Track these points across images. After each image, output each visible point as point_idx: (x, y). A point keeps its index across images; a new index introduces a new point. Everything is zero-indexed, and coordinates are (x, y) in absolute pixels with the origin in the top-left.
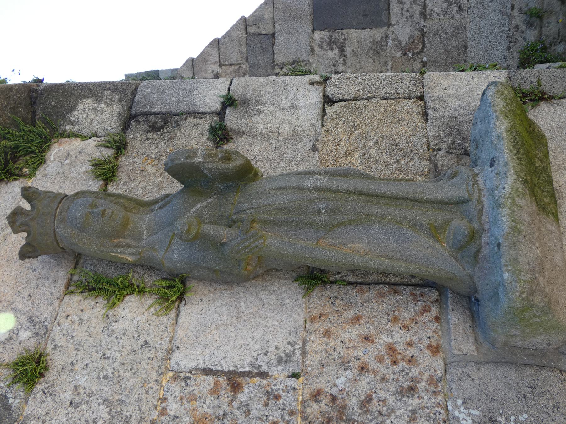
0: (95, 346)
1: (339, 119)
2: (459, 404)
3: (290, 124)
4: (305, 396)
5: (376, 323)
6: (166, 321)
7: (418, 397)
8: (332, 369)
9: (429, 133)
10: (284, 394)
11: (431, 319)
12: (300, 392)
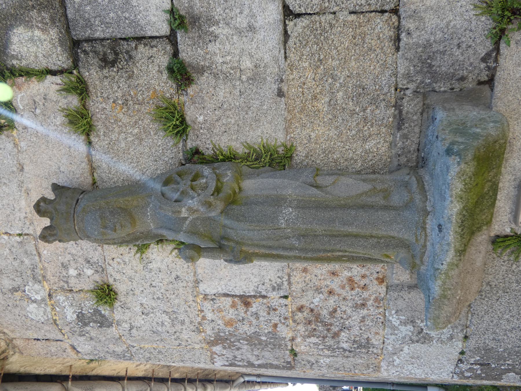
8: (310, 293)
12: (290, 306)
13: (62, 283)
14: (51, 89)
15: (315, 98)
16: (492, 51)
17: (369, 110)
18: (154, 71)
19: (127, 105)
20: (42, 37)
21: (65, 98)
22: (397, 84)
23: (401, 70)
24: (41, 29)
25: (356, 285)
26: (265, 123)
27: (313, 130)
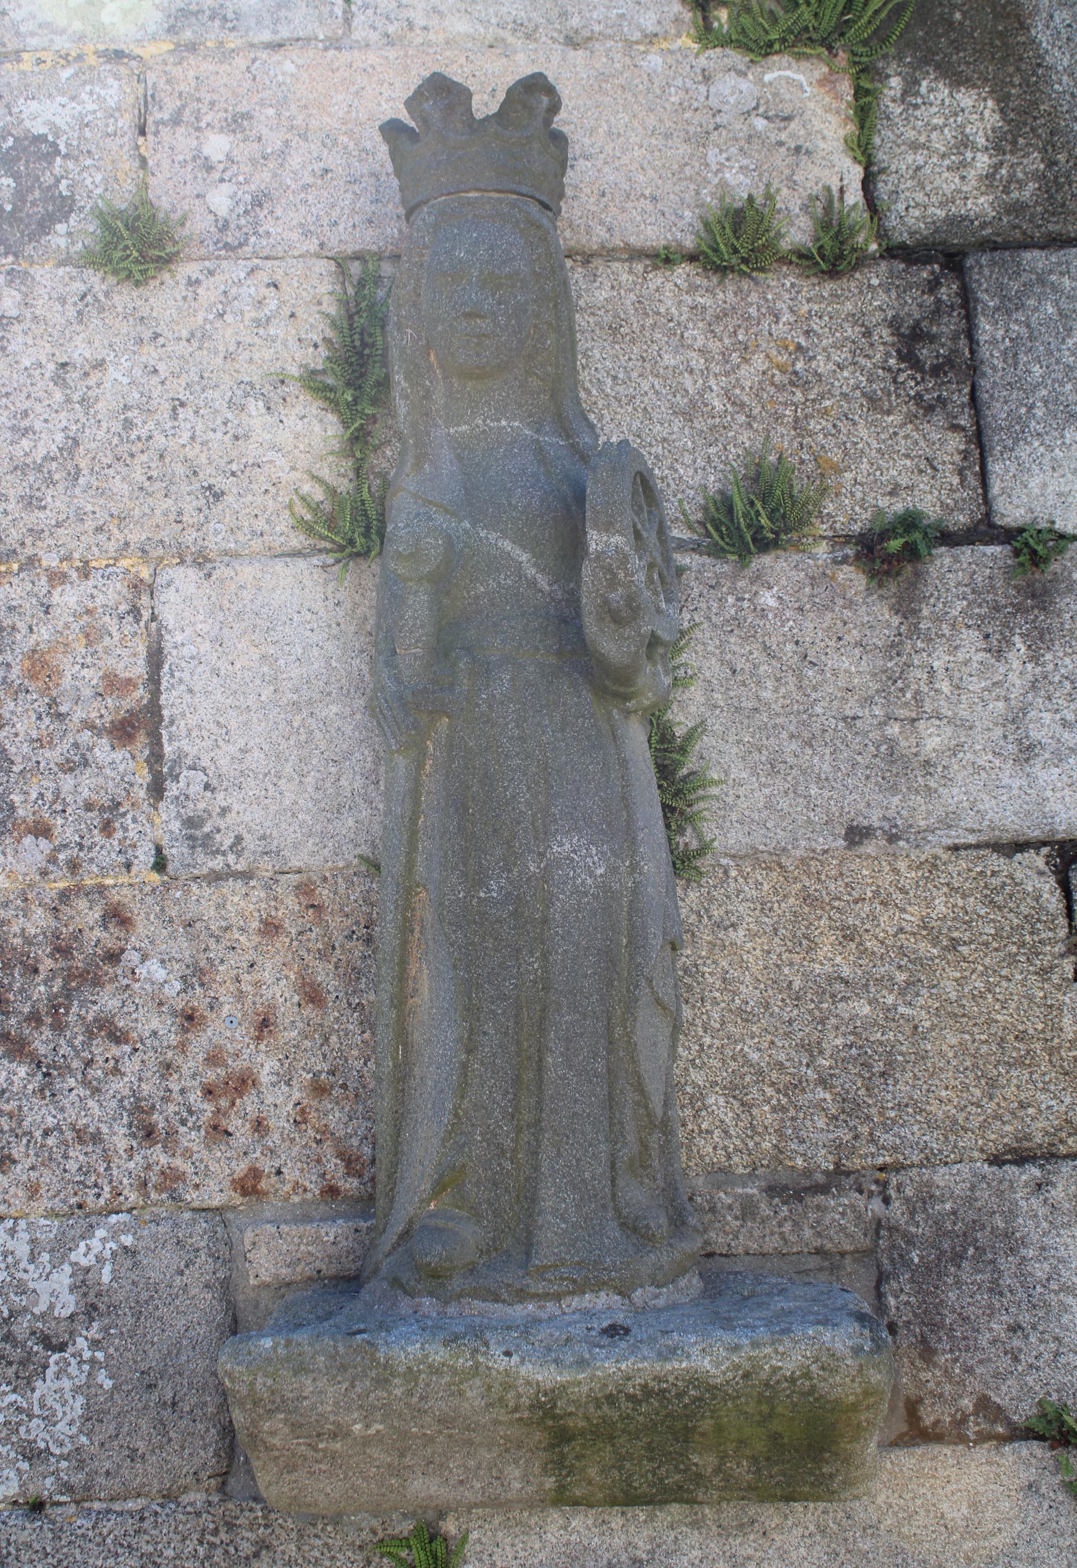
0: (202, 377)
1: (986, 896)
2: (123, 1238)
3: (955, 751)
4: (114, 892)
5: (307, 1044)
6: (278, 529)
7: (132, 1148)
8: (182, 948)
9: (942, 1170)
10: (116, 843)
11: (328, 1177)
12: (124, 879)
13: (171, 105)
14: (827, 172)
15: (849, 935)
16: (1009, 1423)
17: (822, 1096)
18: (895, 473)
19: (792, 383)
20: (973, 172)
21: (805, 208)
22: (898, 1168)
23: (941, 1177)
24: (993, 174)
25: (224, 1103)
26: (767, 791)
27: (752, 935)
